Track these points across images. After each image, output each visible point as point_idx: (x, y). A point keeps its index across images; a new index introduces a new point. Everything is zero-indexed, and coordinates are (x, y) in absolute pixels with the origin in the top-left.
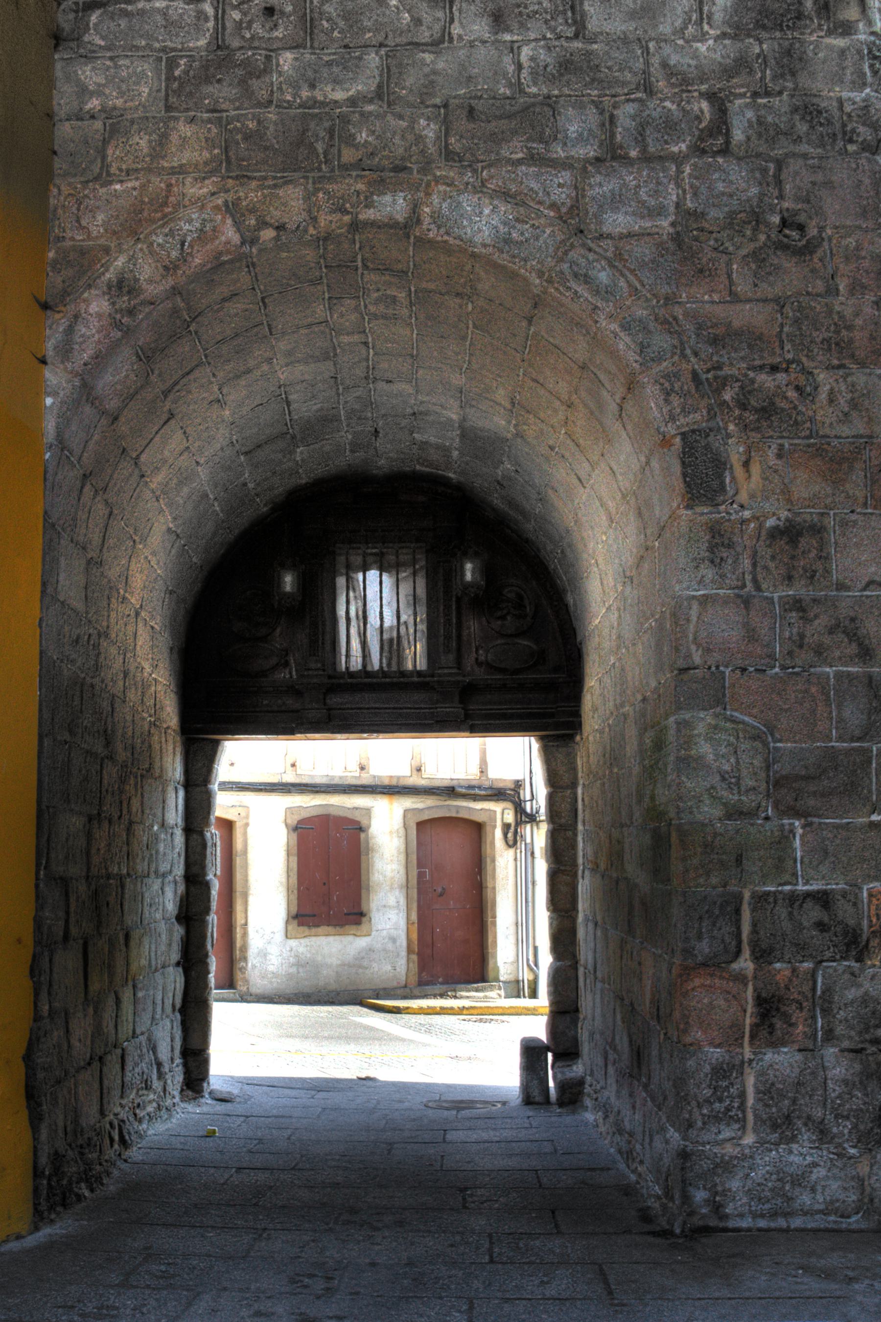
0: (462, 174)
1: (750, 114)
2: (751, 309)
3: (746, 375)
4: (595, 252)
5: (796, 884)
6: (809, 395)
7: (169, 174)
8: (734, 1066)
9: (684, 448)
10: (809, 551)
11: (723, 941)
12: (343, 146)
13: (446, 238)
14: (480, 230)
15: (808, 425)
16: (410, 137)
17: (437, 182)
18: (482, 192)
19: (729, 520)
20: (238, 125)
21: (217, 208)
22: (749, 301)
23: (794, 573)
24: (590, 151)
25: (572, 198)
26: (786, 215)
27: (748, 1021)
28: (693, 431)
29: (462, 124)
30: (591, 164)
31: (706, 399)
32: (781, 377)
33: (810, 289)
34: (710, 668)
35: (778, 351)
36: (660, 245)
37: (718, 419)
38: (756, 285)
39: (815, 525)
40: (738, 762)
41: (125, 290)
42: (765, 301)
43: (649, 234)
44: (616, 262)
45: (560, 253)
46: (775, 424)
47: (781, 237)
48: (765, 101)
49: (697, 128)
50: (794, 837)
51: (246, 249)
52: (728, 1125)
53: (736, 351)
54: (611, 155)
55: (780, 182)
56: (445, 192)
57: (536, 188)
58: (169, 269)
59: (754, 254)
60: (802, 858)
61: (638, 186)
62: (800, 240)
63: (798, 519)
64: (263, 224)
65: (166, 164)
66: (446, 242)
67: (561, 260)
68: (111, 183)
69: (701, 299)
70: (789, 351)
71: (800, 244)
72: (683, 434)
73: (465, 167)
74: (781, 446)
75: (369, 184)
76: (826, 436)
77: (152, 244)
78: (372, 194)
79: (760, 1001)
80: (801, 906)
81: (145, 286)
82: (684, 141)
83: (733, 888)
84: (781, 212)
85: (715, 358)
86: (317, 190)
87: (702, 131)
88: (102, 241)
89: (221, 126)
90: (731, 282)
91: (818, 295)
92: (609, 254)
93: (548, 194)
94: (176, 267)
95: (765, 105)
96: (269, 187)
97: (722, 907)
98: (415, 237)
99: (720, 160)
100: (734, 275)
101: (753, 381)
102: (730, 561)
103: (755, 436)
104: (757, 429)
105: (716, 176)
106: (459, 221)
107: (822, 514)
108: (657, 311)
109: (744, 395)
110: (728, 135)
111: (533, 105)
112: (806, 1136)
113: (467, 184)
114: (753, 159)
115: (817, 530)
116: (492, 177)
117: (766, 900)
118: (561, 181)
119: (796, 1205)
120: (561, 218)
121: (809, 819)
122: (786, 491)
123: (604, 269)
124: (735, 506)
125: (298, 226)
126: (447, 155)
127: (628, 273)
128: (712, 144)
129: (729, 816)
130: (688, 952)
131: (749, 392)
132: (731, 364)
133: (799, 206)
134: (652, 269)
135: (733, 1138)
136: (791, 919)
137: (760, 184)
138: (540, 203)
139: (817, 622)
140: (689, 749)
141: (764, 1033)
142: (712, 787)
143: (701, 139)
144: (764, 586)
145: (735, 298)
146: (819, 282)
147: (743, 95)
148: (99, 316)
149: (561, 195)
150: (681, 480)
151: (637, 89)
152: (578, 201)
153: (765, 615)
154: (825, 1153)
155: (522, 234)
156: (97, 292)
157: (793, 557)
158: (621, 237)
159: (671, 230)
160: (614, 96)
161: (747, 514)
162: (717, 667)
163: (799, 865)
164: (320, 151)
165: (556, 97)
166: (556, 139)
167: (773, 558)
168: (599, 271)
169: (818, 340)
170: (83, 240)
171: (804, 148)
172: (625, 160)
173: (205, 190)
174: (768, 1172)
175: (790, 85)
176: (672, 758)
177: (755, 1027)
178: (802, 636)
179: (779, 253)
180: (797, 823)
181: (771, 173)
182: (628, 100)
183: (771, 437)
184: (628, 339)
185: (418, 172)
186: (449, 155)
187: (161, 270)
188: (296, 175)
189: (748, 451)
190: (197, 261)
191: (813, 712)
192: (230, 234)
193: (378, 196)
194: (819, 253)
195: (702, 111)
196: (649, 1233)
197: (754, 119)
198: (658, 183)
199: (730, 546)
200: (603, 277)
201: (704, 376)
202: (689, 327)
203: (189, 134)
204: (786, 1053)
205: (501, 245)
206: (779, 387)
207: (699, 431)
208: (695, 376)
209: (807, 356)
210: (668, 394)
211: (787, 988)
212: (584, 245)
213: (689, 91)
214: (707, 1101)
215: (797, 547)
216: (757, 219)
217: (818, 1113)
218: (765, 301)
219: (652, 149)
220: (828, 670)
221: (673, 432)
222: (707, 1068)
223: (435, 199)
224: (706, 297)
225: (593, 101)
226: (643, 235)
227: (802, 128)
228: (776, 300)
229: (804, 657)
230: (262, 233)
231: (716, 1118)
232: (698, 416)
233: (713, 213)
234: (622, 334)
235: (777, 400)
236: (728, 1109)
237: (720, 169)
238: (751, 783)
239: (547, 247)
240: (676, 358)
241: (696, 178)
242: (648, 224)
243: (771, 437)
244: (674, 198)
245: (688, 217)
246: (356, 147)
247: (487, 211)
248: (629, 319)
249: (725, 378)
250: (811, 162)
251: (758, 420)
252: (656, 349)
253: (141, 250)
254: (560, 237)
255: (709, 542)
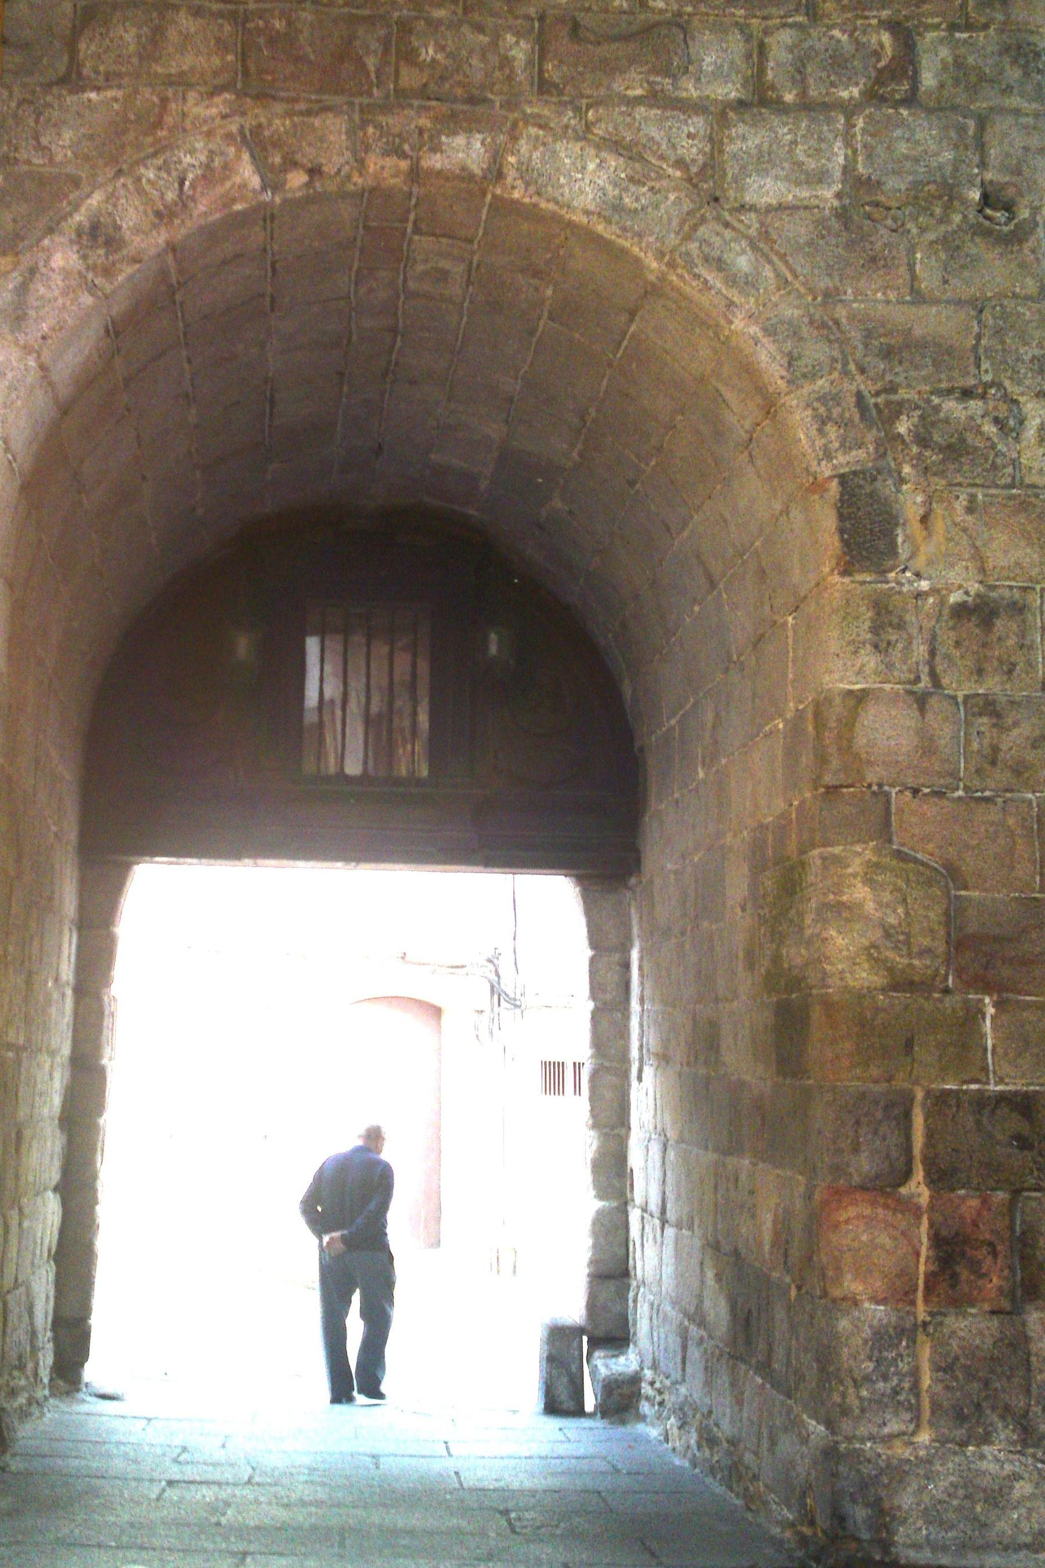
0: (560, 114)
1: (944, 52)
2: (939, 313)
3: (928, 401)
4: (734, 229)
5: (988, 1083)
6: (1012, 430)
7: (164, 83)
8: (903, 1330)
9: (842, 495)
10: (1008, 637)
11: (888, 1156)
12: (402, 63)
13: (535, 199)
14: (582, 192)
15: (1009, 470)
16: (494, 59)
17: (527, 123)
18: (585, 138)
19: (900, 593)
20: (261, 23)
21: (229, 137)
22: (937, 302)
23: (986, 665)
24: (730, 91)
25: (705, 154)
26: (990, 189)
27: (922, 1268)
28: (855, 473)
29: (562, 43)
30: (732, 109)
31: (874, 431)
32: (975, 406)
33: (1018, 290)
34: (870, 786)
35: (972, 369)
36: (821, 222)
37: (890, 459)
38: (946, 282)
39: (1015, 603)
40: (907, 914)
41: (101, 240)
42: (959, 303)
43: (806, 208)
44: (762, 243)
45: (686, 228)
46: (966, 468)
47: (981, 219)
48: (965, 35)
49: (875, 67)
50: (984, 1019)
51: (267, 196)
52: (896, 1413)
53: (917, 368)
54: (759, 99)
55: (983, 145)
56: (537, 138)
57: (657, 138)
58: (164, 216)
59: (944, 241)
60: (994, 1047)
61: (794, 142)
62: (1006, 224)
63: (993, 594)
64: (291, 163)
65: (160, 70)
66: (535, 205)
67: (688, 238)
68: (83, 90)
69: (874, 298)
70: (986, 371)
71: (1005, 229)
72: (843, 479)
73: (564, 104)
74: (972, 498)
75: (436, 119)
76: (1034, 486)
77: (139, 179)
78: (440, 133)
79: (937, 1240)
80: (993, 1112)
81: (127, 235)
82: (857, 84)
83: (901, 1082)
84: (983, 183)
85: (888, 378)
86: (364, 124)
87: (880, 71)
88: (71, 169)
89: (236, 24)
90: (914, 277)
91: (1027, 298)
92: (752, 232)
93: (674, 147)
94: (172, 215)
95: (965, 41)
96: (301, 113)
97: (886, 1108)
98: (494, 196)
99: (905, 112)
100: (918, 267)
101: (937, 409)
102: (900, 646)
103: (939, 483)
104: (941, 474)
105: (898, 132)
106: (554, 179)
107: (1025, 589)
108: (812, 311)
109: (924, 426)
110: (915, 80)
111: (657, 24)
112: (1005, 1434)
113: (567, 127)
114: (948, 113)
115: (1018, 609)
116: (599, 120)
117: (945, 1102)
118: (692, 130)
119: (992, 1535)
120: (689, 180)
121: (1005, 995)
122: (979, 557)
123: (743, 252)
124: (908, 574)
125: (339, 170)
126: (540, 87)
127: (775, 259)
128: (894, 90)
129: (895, 987)
130: (838, 1170)
131: (933, 424)
132: (909, 386)
133: (1007, 179)
134: (808, 254)
135: (904, 1433)
136: (979, 1130)
137: (956, 146)
138: (662, 158)
139: (1015, 732)
140: (841, 893)
141: (943, 1288)
142: (873, 946)
143: (879, 81)
144: (945, 681)
145: (919, 298)
146: (1030, 282)
147: (937, 27)
148: (66, 273)
149: (692, 150)
150: (836, 538)
151: (797, 10)
152: (712, 157)
153: (946, 719)
154: (1030, 1461)
155: (637, 200)
156: (62, 239)
157: (984, 645)
158: (769, 209)
159: (836, 203)
160: (765, 18)
161: (924, 585)
162: (880, 786)
163: (989, 1056)
164: (372, 68)
165: (689, 15)
166: (686, 71)
167: (958, 644)
168: (738, 254)
169: (1027, 358)
170: (44, 165)
171: (1015, 101)
172: (780, 107)
173: (214, 111)
174: (952, 1484)
175: (1000, 17)
176: (813, 904)
177: (930, 1277)
178: (995, 749)
179: (978, 240)
180: (987, 1000)
181: (971, 133)
182: (784, 25)
183: (960, 484)
184: (772, 348)
185: (501, 106)
186: (544, 87)
187: (151, 216)
188: (339, 100)
189: (929, 501)
190: (202, 208)
191: (1012, 851)
192: (247, 174)
193: (448, 136)
194: (1031, 243)
195: (882, 46)
196: (344, 709)
197: (950, 60)
198: (821, 140)
199: (901, 626)
200: (743, 263)
201: (873, 401)
202: (855, 335)
203: (192, 30)
204: (974, 1316)
205: (607, 213)
206: (972, 418)
207: (863, 472)
208: (859, 396)
209: (1011, 378)
210: (823, 423)
211: (975, 1224)
212: (718, 218)
213: (867, 18)
214: (867, 1379)
215: (990, 631)
216: (949, 193)
217: (1019, 1402)
218: (959, 303)
219: (813, 93)
220: (1030, 796)
221: (828, 473)
222: (867, 1332)
223: (524, 146)
224: (879, 295)
225: (737, 24)
226: (798, 208)
227: (1014, 74)
228: (972, 302)
229: (1001, 777)
230: (289, 176)
231: (879, 1403)
232: (860, 454)
233: (892, 183)
234: (765, 340)
235: (969, 437)
236: (896, 1392)
237: (902, 123)
238: (926, 942)
239: (670, 220)
240: (836, 375)
241: (873, 135)
242: (806, 194)
243: (960, 484)
244: (841, 160)
245: (859, 187)
246: (421, 66)
247: (591, 166)
248: (774, 321)
249: (901, 404)
250: (1024, 120)
251: (943, 461)
252: (810, 362)
253: (124, 185)
254: (687, 205)
255: (873, 621)
